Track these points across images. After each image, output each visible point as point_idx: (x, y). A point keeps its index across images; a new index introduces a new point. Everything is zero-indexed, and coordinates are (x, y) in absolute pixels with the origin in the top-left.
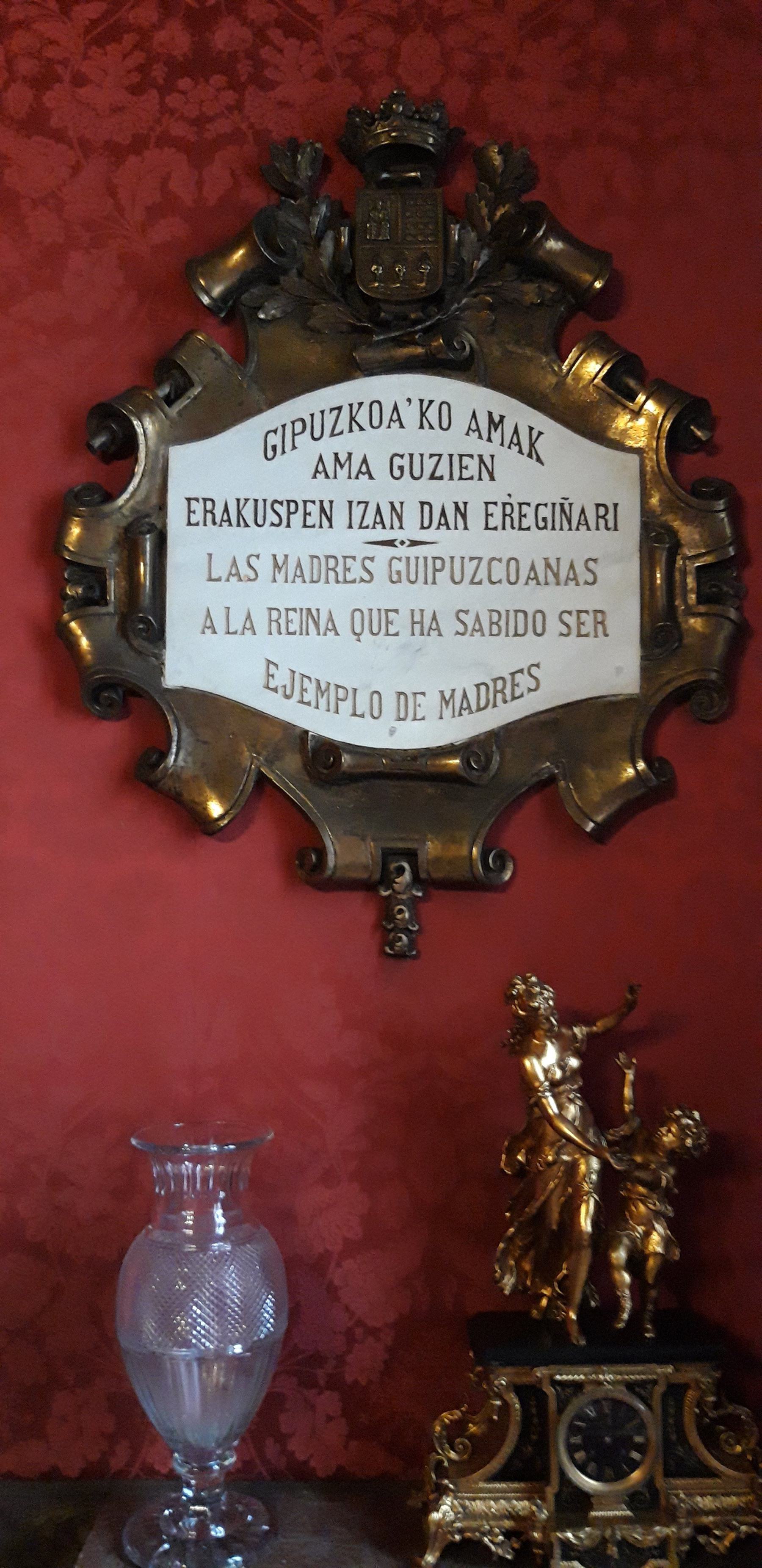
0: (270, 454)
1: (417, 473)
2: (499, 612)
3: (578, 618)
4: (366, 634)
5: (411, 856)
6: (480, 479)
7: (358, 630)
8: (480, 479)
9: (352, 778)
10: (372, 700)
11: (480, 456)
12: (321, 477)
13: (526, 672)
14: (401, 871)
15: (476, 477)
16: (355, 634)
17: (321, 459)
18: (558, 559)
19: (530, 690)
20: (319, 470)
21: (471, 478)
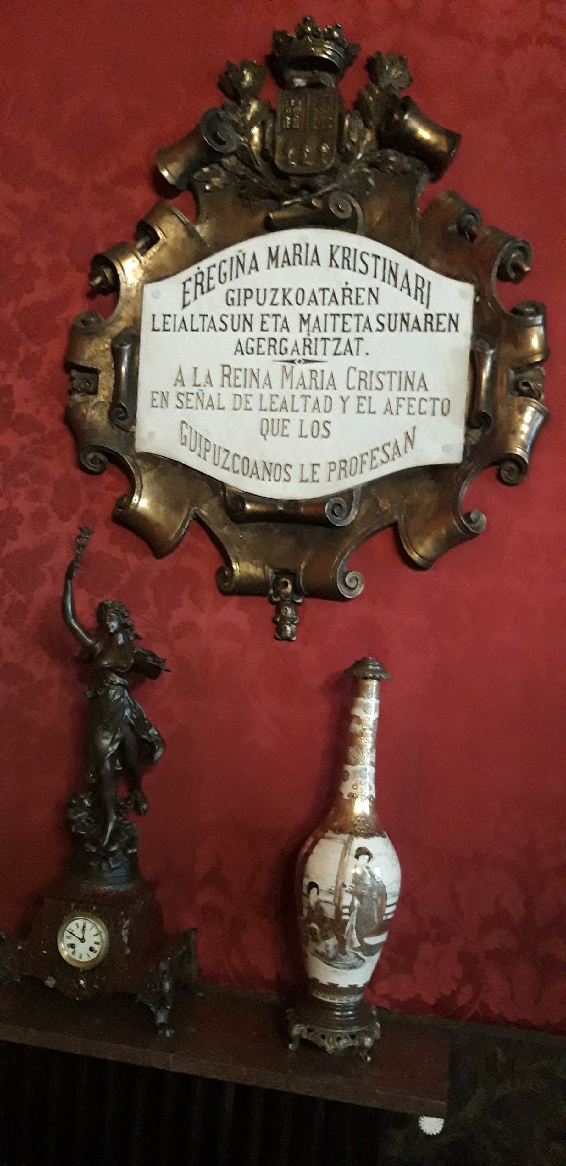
0: (223, 279)
1: (392, 327)
2: (251, 291)
3: (409, 402)
4: (269, 436)
5: (293, 576)
6: (449, 330)
7: (264, 432)
8: (449, 330)
9: (254, 517)
10: (262, 424)
11: (370, 290)
12: (239, 354)
13: (381, 450)
14: (286, 584)
15: (447, 329)
16: (262, 435)
17: (239, 343)
18: (414, 372)
19: (383, 462)
20: (240, 349)
21: (444, 331)
